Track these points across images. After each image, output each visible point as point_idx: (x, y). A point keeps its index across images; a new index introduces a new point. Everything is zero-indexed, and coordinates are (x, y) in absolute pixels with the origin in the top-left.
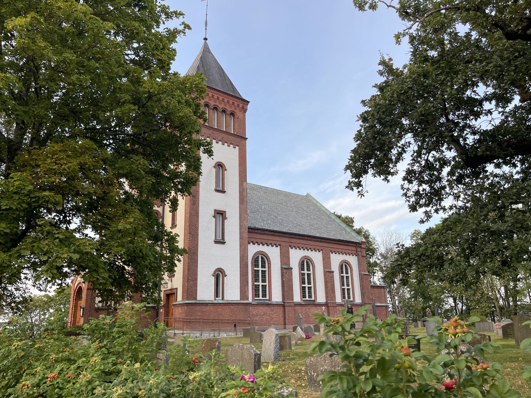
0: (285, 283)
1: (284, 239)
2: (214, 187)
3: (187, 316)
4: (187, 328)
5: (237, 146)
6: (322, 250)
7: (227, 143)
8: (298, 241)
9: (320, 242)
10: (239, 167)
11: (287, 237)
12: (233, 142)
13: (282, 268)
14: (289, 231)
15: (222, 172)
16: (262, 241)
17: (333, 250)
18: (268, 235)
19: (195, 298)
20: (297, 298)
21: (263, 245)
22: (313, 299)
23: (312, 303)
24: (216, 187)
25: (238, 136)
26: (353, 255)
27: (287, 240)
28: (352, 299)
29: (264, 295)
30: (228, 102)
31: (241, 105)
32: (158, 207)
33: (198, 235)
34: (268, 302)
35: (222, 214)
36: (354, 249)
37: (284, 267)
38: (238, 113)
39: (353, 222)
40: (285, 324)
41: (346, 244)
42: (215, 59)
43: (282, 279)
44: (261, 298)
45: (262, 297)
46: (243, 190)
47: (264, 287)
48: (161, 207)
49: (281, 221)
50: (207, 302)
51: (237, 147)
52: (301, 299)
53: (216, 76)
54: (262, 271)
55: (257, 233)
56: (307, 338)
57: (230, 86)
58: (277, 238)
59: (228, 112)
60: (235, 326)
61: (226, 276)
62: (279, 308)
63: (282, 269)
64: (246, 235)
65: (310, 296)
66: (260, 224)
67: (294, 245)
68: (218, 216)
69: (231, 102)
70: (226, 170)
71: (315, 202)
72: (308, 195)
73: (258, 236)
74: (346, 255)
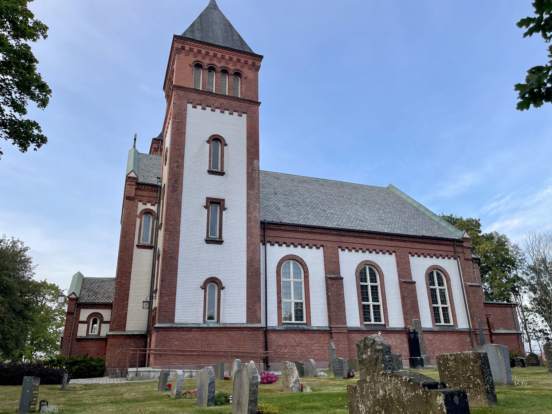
1: (330, 238)
2: (207, 168)
5: (244, 113)
6: (394, 252)
7: (228, 110)
8: (352, 240)
9: (391, 240)
10: (247, 140)
11: (334, 235)
12: (237, 109)
13: (326, 277)
16: (293, 241)
17: (413, 251)
18: (302, 232)
19: (172, 321)
20: (427, 322)
22: (383, 322)
23: (450, 329)
25: (245, 100)
26: (449, 258)
27: (334, 238)
28: (452, 323)
30: (231, 59)
31: (250, 62)
32: (152, 205)
33: (179, 233)
35: (219, 203)
36: (451, 249)
38: (246, 72)
39: (479, 225)
41: (435, 242)
42: (223, 16)
43: (327, 294)
44: (373, 322)
45: (296, 320)
46: (253, 170)
51: (245, 116)
52: (361, 323)
57: (239, 42)
58: (318, 237)
59: (230, 72)
62: (322, 335)
63: (327, 279)
64: (257, 231)
65: (447, 320)
67: (346, 245)
70: (226, 145)
71: (399, 193)
72: (391, 186)
73: (286, 234)
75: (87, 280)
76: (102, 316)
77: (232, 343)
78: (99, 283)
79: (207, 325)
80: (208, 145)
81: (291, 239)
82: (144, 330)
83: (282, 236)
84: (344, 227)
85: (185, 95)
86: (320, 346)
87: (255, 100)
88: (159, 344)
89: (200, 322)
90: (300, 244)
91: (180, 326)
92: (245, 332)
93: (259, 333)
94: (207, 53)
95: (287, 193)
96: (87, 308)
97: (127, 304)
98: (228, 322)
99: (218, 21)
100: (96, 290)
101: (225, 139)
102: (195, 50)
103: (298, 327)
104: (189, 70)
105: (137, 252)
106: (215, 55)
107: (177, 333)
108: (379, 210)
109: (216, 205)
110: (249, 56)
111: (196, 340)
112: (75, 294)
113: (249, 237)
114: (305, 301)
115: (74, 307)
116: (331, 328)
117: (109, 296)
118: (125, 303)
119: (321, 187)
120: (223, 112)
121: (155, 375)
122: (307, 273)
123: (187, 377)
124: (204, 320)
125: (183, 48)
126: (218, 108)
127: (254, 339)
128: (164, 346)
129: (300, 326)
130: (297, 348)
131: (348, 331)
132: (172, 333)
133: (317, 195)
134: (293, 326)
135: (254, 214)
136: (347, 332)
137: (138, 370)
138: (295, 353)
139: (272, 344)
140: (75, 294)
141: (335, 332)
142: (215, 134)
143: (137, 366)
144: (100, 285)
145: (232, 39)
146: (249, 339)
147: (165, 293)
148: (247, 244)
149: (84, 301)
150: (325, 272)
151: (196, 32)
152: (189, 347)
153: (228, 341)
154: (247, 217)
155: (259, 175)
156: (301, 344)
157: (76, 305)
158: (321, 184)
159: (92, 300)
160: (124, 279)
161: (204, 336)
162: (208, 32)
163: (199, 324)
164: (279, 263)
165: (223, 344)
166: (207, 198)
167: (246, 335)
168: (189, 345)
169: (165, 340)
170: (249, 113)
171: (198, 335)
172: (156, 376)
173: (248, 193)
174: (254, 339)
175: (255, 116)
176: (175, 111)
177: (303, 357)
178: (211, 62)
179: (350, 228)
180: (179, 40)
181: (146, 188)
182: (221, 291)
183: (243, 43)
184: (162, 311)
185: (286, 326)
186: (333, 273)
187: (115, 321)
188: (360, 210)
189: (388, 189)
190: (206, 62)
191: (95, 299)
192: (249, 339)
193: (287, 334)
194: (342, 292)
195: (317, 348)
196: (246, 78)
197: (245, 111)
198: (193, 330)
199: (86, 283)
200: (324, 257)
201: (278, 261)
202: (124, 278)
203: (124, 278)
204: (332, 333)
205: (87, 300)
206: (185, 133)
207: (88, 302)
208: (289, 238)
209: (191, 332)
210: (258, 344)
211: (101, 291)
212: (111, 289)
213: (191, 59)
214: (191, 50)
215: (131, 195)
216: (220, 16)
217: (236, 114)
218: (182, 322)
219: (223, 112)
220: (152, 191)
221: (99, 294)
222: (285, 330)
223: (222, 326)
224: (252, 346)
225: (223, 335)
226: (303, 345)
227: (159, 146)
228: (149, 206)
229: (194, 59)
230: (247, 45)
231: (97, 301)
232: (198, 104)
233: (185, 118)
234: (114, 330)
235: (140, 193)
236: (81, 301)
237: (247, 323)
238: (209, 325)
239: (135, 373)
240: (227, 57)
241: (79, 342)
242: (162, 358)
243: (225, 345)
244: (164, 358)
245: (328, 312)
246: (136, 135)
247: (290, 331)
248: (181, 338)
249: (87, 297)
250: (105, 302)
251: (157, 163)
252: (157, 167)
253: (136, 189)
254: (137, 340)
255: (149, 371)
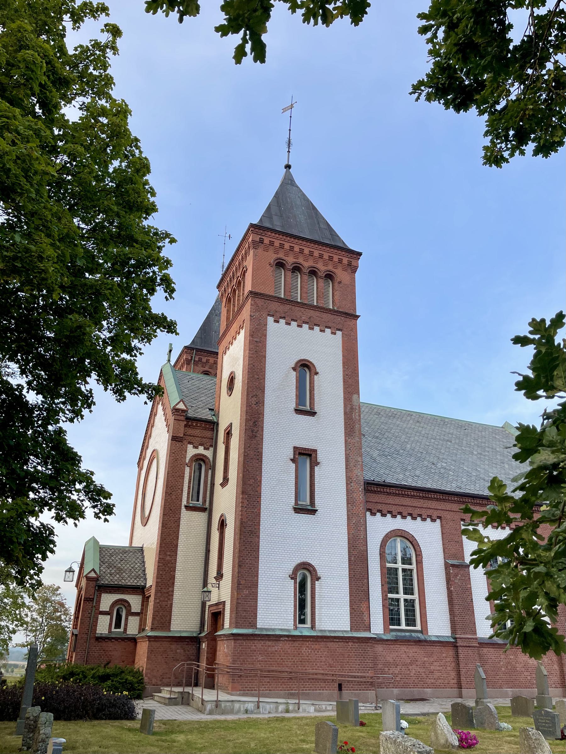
0: (454, 594)
1: (449, 506)
2: (293, 405)
3: (234, 662)
4: (234, 689)
5: (339, 330)
7: (318, 325)
10: (344, 367)
12: (330, 325)
13: (446, 564)
14: (458, 490)
15: (310, 377)
16: (400, 509)
18: (413, 497)
19: (253, 625)
21: (404, 517)
22: (418, 628)
24: (297, 404)
29: (411, 621)
30: (321, 256)
31: (345, 261)
32: (205, 449)
33: (259, 496)
34: (420, 635)
35: (310, 455)
37: (450, 562)
38: (341, 274)
40: (460, 686)
42: (304, 195)
43: (448, 589)
45: (407, 625)
46: (352, 408)
47: (410, 604)
48: (212, 449)
49: (442, 471)
50: (278, 633)
51: (339, 333)
53: (302, 218)
54: (404, 570)
55: (389, 494)
56: (461, 747)
57: (327, 233)
59: (320, 274)
60: (340, 687)
61: (318, 579)
62: (444, 649)
64: (360, 496)
66: (396, 476)
68: (301, 459)
69: (326, 256)
70: (317, 373)
73: (391, 500)
74: (424, 520)
75: (104, 549)
76: (129, 605)
77: (333, 660)
78: (121, 555)
79: (301, 633)
80: (295, 373)
81: (398, 506)
82: (195, 630)
83: (386, 502)
84: (468, 491)
85: (265, 305)
86: (442, 666)
87: (351, 312)
88: (238, 658)
89: (290, 628)
90: (410, 515)
91: (265, 633)
92: (350, 644)
93: (368, 646)
94: (292, 248)
95: (377, 434)
96: (110, 593)
97: (173, 591)
98: (326, 629)
99: (298, 203)
100: (119, 565)
101: (316, 365)
102: (277, 243)
103: (411, 636)
104: (270, 271)
105: (185, 515)
106: (301, 251)
107: (260, 643)
108: (504, 463)
109: (305, 457)
110: (344, 253)
111: (286, 654)
112: (95, 572)
113: (350, 505)
114: (418, 597)
115: (93, 591)
116: (455, 638)
117: (137, 575)
118: (170, 589)
119: (418, 424)
120: (313, 329)
121: (240, 707)
122: (421, 557)
123: (282, 712)
124: (295, 625)
125: (261, 241)
126: (306, 323)
127: (362, 655)
128: (244, 661)
129: (413, 634)
130: (410, 667)
131: (479, 643)
132: (254, 643)
133: (416, 438)
134: (403, 634)
135: (356, 471)
136: (477, 645)
137: (219, 699)
138: (409, 674)
139: (377, 660)
140: (95, 572)
141: (462, 644)
142: (302, 358)
143: (184, 684)
144: (123, 557)
145: (320, 227)
146: (355, 655)
147: (244, 584)
148: (348, 515)
149: (106, 582)
150: (444, 555)
151: (275, 218)
152: (278, 664)
153: (328, 657)
154: (346, 476)
155: (360, 416)
156: (417, 661)
157: (97, 588)
158: (416, 419)
159: (116, 580)
160: (169, 555)
161: (296, 649)
162: (289, 218)
163: (288, 630)
164: (382, 541)
165: (321, 662)
166: (295, 448)
167: (351, 648)
168: (276, 661)
169: (246, 653)
170: (345, 329)
171: (287, 646)
172: (242, 709)
173: (346, 441)
174: (362, 655)
175: (352, 334)
176: (252, 327)
177: (420, 681)
178: (296, 260)
179: (476, 493)
180: (257, 230)
181: (199, 425)
182: (316, 582)
183: (334, 233)
184: (241, 611)
185: (394, 633)
186: (455, 557)
187: (157, 616)
188: (478, 463)
189: (504, 430)
190: (290, 260)
191: (120, 578)
192: (355, 655)
193: (397, 646)
194: (469, 586)
195: (438, 668)
196: (340, 283)
197: (340, 327)
198: (282, 639)
199: (104, 554)
200: (442, 533)
201: (381, 539)
202: (169, 553)
203: (169, 553)
204: (457, 647)
205: (109, 580)
206: (265, 357)
207: (112, 583)
208: (396, 505)
209: (279, 642)
210: (368, 662)
211: (126, 568)
212: (139, 564)
213: (272, 257)
214: (271, 243)
215: (179, 435)
216: (300, 195)
217: (328, 331)
218: (266, 627)
219: (313, 329)
220: (205, 429)
221: (124, 572)
222: (395, 640)
223: (319, 634)
224: (359, 665)
225: (322, 647)
226: (418, 663)
227: (192, 357)
228: (201, 450)
229: (275, 256)
230: (338, 236)
231: (123, 582)
232: (281, 318)
233: (266, 336)
234: (156, 629)
235: (190, 431)
236: (103, 582)
237: (351, 631)
238: (301, 633)
239: (214, 703)
240: (316, 253)
241: (99, 642)
242: (242, 680)
243: (324, 662)
244: (245, 680)
245: (450, 615)
246: (171, 345)
247: (401, 642)
248: (266, 651)
249: (109, 575)
250: (134, 584)
251: (202, 386)
252: (203, 391)
253: (186, 426)
254: (187, 645)
255: (232, 701)
